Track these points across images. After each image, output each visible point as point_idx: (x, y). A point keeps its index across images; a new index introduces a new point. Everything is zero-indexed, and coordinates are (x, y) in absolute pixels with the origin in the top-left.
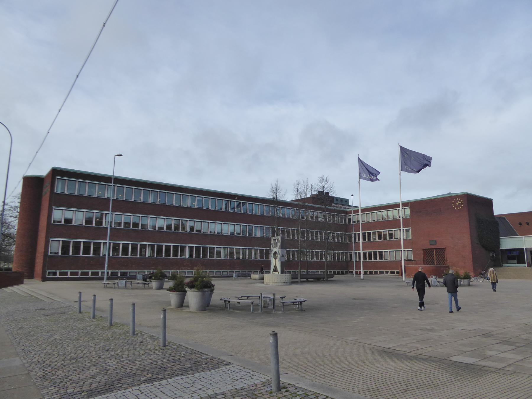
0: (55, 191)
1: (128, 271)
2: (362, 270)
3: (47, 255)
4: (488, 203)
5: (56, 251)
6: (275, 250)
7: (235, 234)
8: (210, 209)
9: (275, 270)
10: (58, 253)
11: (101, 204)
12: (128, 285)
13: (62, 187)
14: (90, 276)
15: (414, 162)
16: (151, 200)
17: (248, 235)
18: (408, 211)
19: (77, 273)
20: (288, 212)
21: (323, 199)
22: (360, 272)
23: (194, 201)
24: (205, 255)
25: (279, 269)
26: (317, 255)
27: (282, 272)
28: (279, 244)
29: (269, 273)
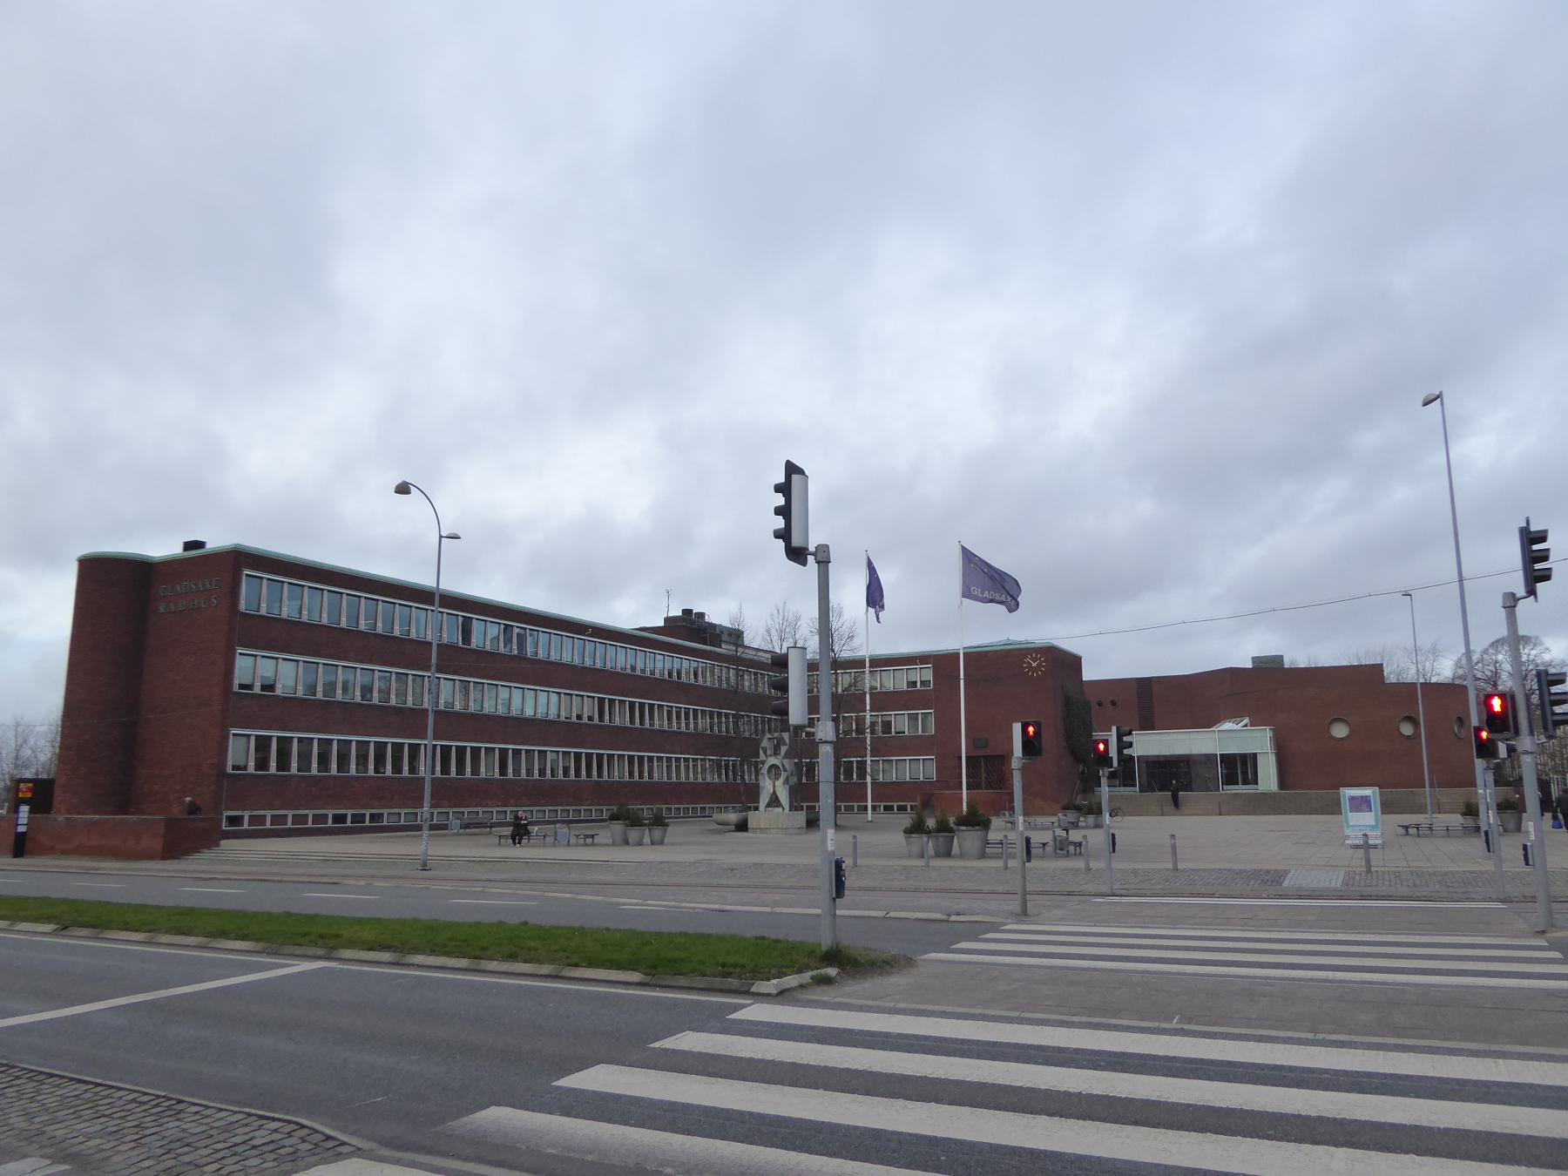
0: (242, 607)
1: (385, 812)
2: (869, 805)
3: (225, 774)
4: (1072, 663)
5: (242, 764)
6: (773, 761)
7: (257, 690)
8: (263, 612)
9: (774, 801)
10: (245, 768)
11: (405, 653)
12: (647, 840)
13: (256, 595)
14: (268, 825)
15: (991, 583)
16: (287, 611)
17: (358, 699)
18: (928, 675)
19: (262, 819)
20: (621, 659)
21: (690, 629)
22: (866, 808)
23: (336, 611)
24: (283, 763)
25: (784, 797)
26: (727, 766)
27: (793, 808)
28: (784, 749)
29: (757, 809)
